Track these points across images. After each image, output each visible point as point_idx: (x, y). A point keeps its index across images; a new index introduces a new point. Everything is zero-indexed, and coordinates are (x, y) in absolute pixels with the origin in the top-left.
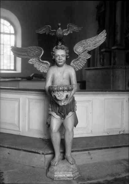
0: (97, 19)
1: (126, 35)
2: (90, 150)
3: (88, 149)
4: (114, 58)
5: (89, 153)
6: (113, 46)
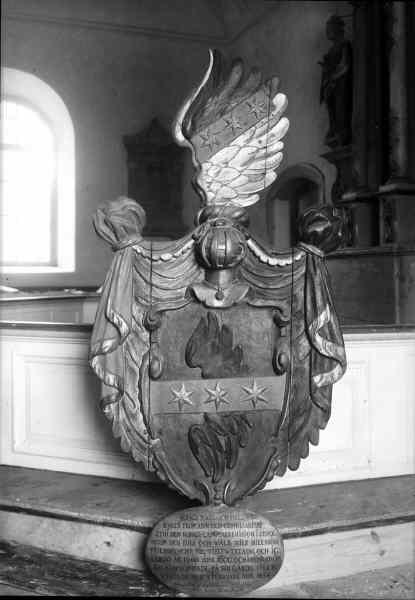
0: (322, 98)
2: (379, 526)
3: (370, 522)
4: (389, 221)
5: (373, 534)
6: (383, 184)
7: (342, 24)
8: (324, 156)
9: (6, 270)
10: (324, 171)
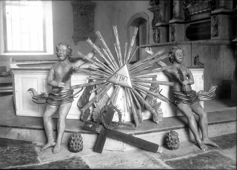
1: (186, 6)
4: (173, 33)
6: (171, 19)
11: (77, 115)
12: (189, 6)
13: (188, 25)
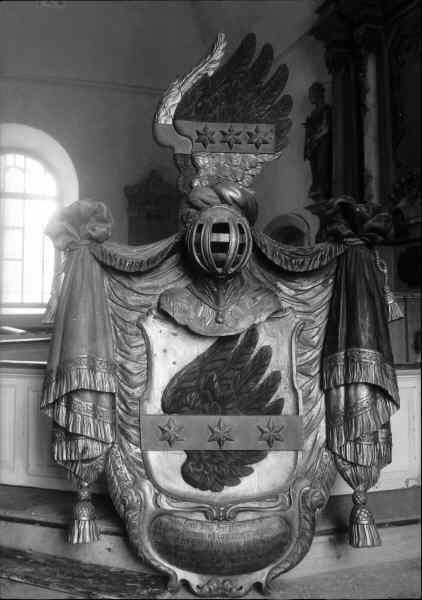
0: (306, 157)
1: (396, 203)
7: (323, 90)
8: (308, 208)
9: (7, 311)
10: (309, 221)
11: (7, 259)
12: (402, 204)
13: (402, 249)
